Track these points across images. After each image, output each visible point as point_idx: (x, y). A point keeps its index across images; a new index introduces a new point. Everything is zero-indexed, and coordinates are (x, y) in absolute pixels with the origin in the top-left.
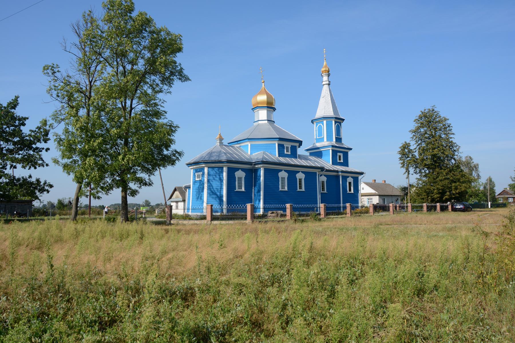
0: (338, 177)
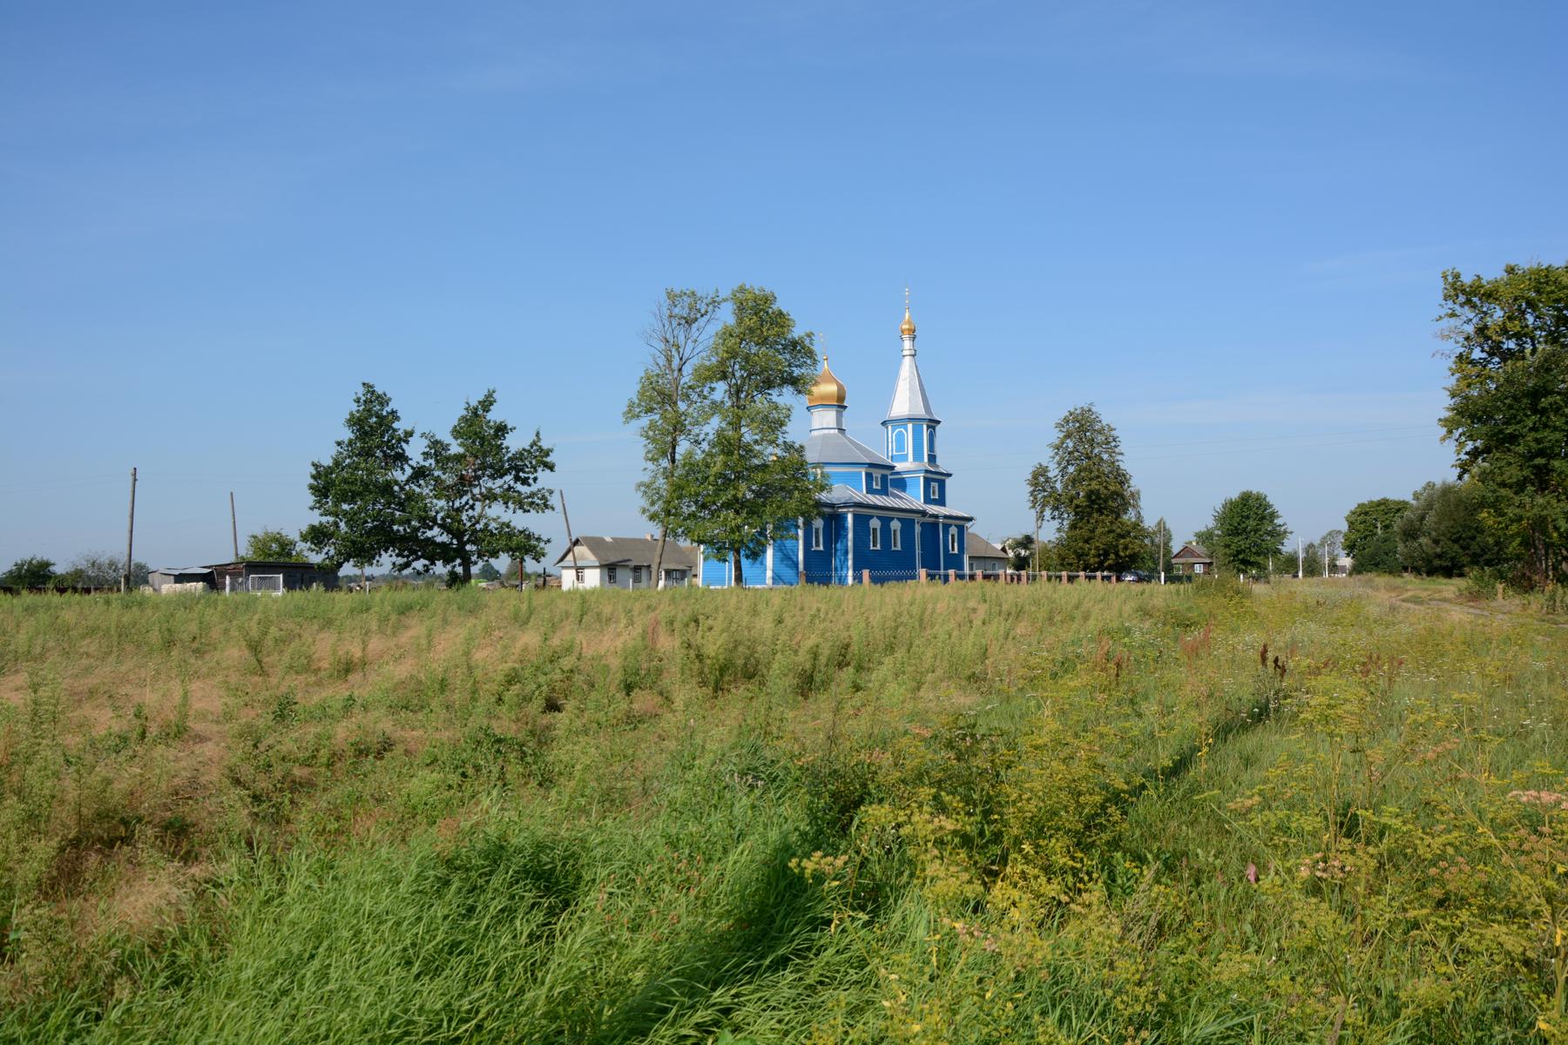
0: (936, 525)
